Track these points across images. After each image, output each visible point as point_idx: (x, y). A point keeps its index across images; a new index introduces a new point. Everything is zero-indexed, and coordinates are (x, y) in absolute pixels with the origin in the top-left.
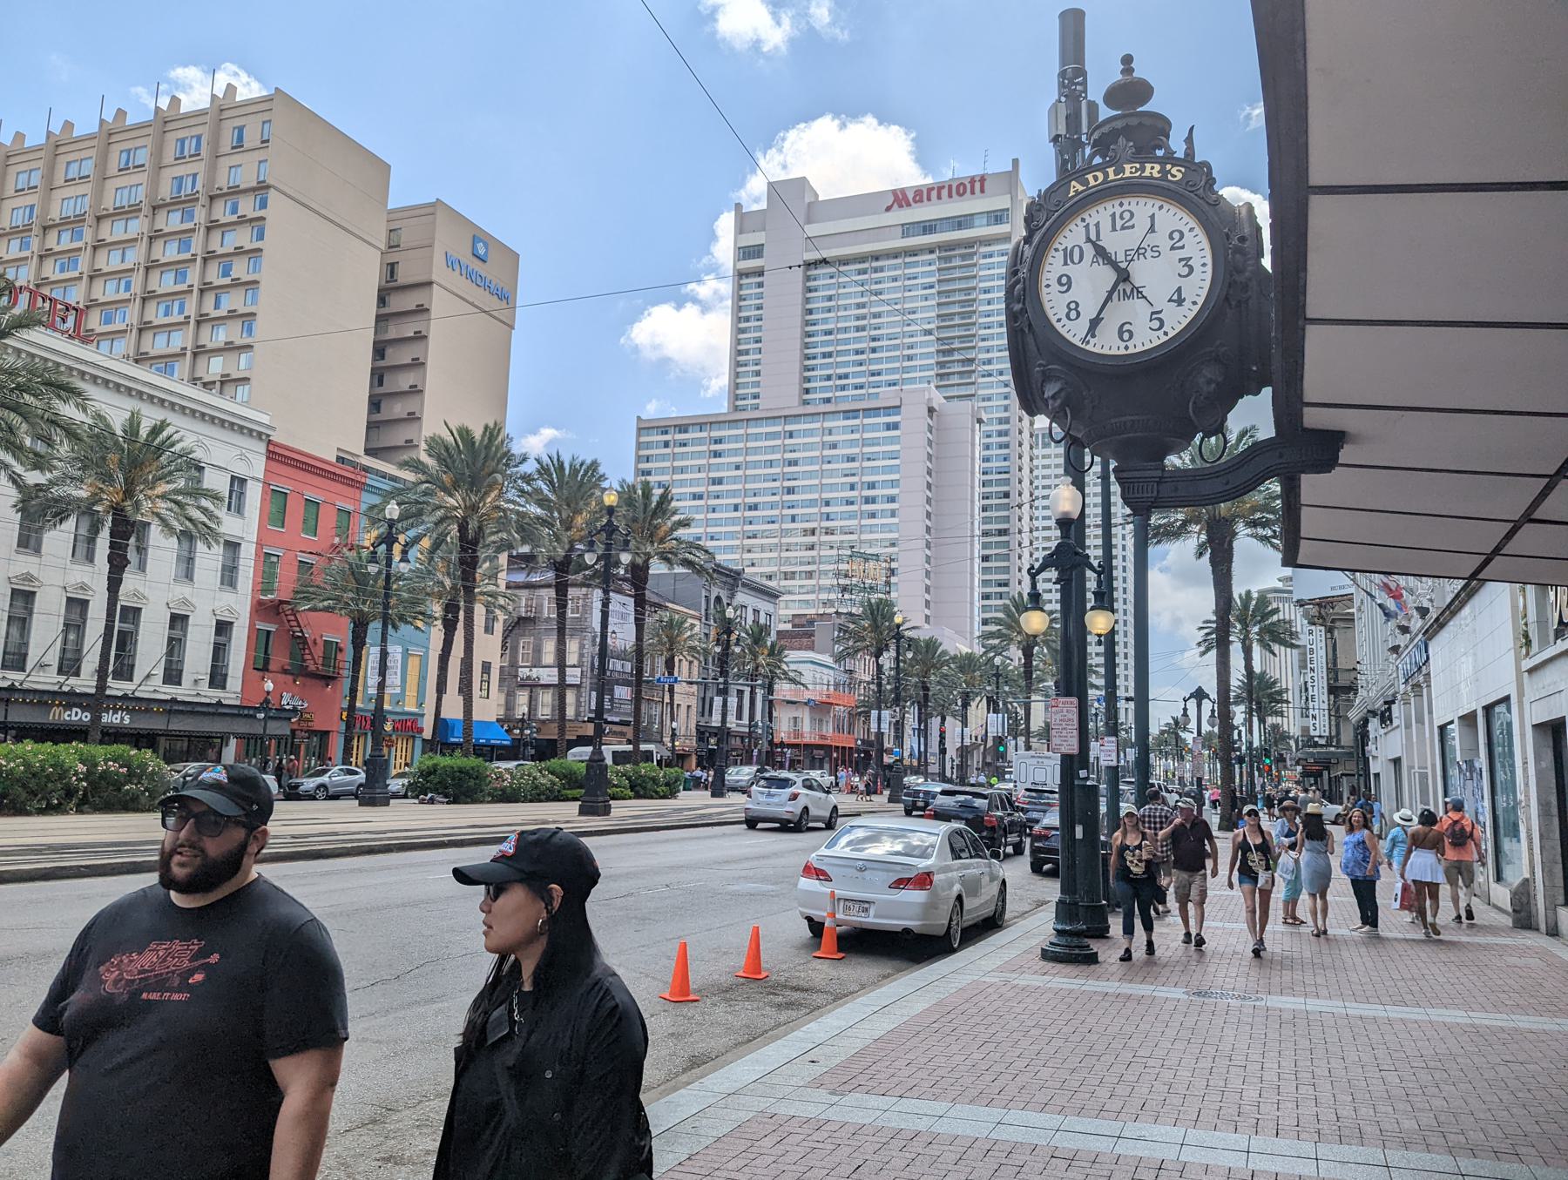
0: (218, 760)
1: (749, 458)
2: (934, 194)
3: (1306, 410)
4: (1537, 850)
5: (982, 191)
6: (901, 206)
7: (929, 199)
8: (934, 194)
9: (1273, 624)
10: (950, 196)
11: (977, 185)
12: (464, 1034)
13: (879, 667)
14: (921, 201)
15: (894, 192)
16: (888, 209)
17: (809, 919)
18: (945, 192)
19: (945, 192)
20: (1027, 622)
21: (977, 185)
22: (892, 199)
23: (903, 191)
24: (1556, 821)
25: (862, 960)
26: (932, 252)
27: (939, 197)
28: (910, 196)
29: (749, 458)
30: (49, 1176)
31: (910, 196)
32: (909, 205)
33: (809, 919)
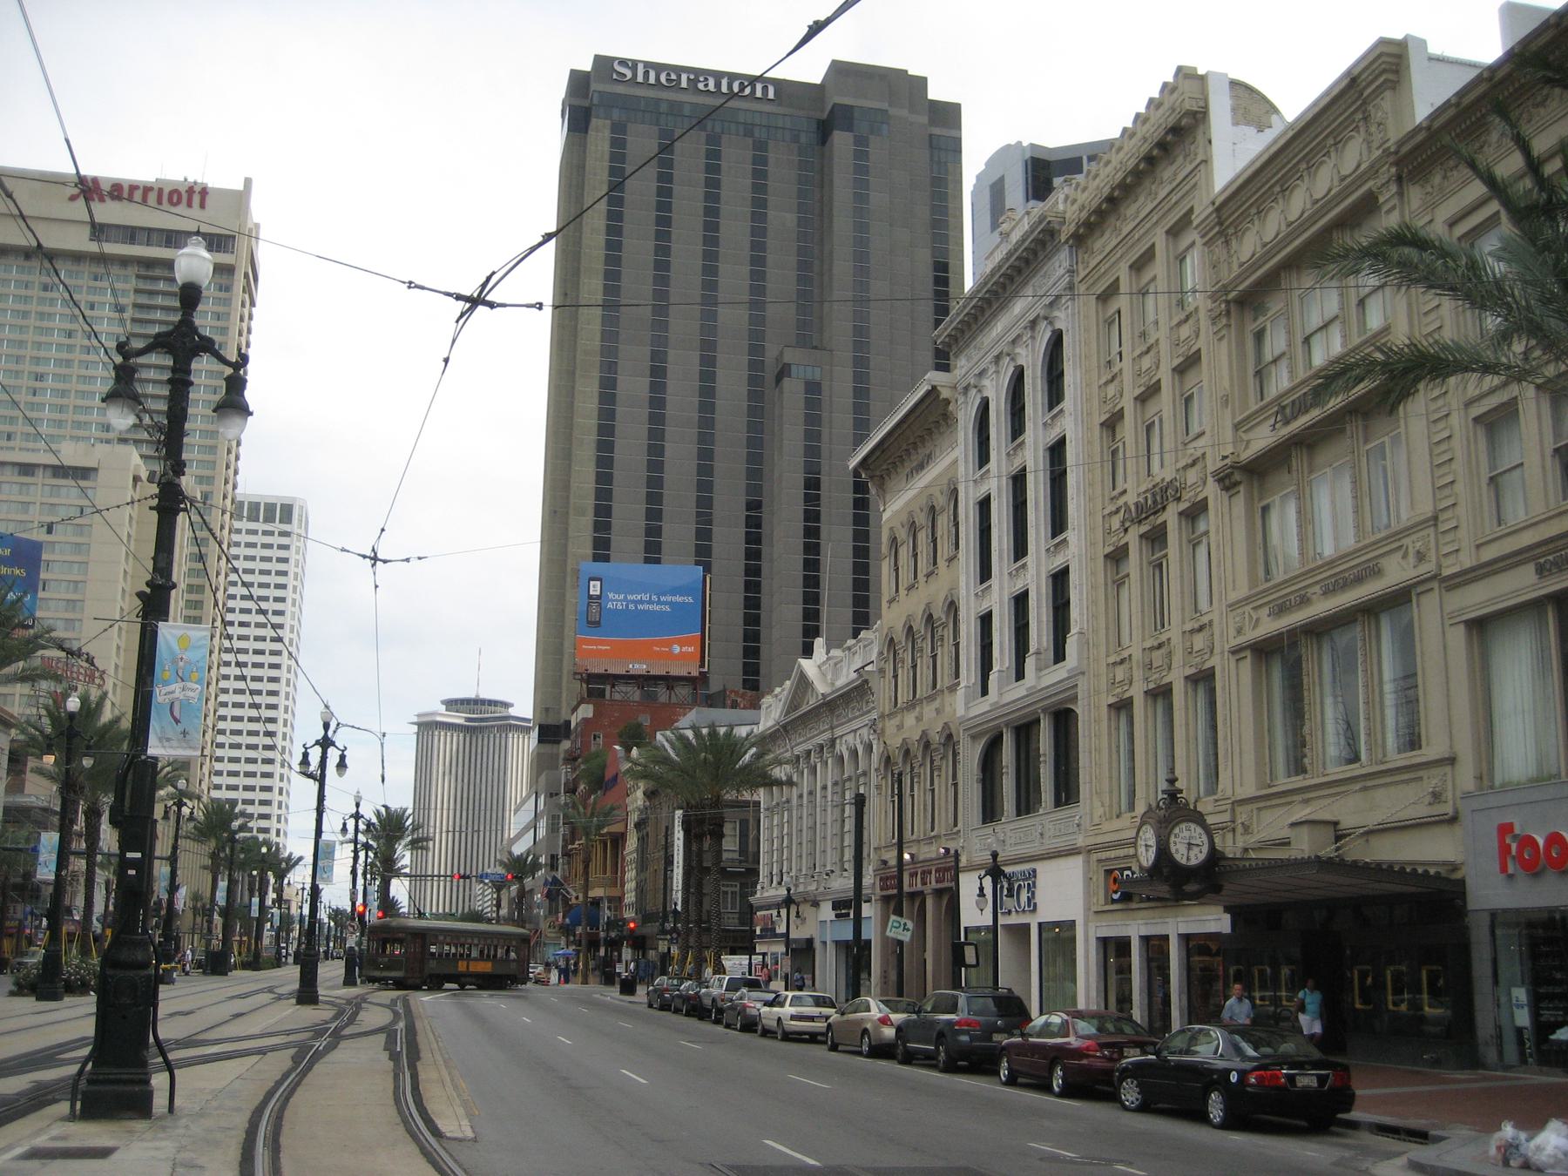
5: (202, 206)
11: (196, 199)
18: (152, 198)
21: (196, 199)
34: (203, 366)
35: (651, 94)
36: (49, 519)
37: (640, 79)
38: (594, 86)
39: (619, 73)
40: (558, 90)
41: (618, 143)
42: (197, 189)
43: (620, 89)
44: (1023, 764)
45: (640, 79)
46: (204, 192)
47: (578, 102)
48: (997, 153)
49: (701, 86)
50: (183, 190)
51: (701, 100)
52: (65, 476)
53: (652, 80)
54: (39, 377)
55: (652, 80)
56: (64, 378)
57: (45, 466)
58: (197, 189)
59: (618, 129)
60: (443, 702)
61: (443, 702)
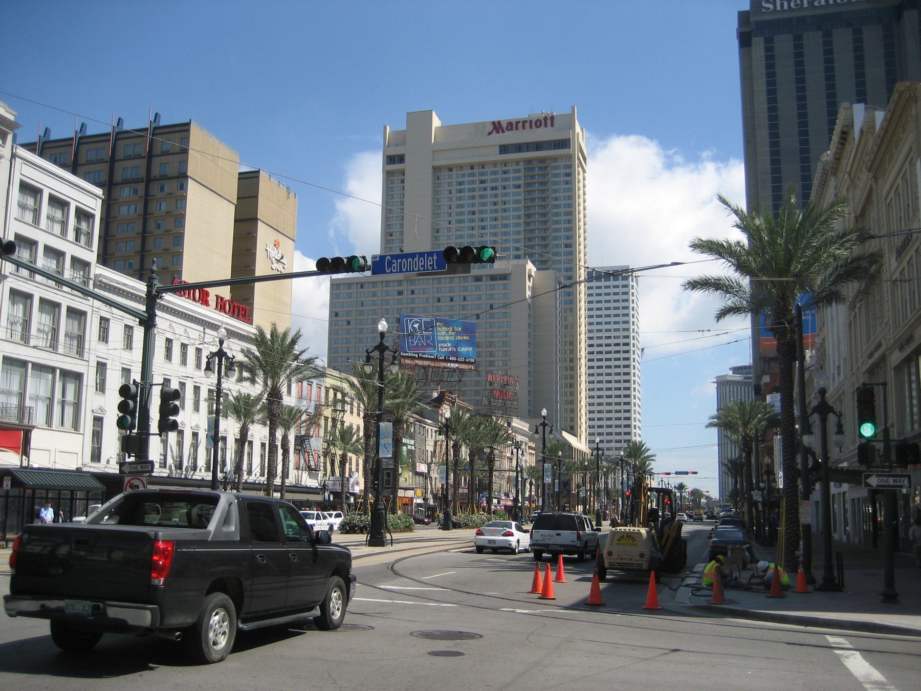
0: (329, 367)
2: (520, 125)
5: (552, 125)
7: (517, 129)
8: (520, 125)
10: (531, 127)
11: (549, 122)
12: (871, 664)
13: (674, 154)
14: (512, 129)
15: (493, 123)
17: (707, 427)
18: (527, 125)
19: (527, 125)
21: (549, 122)
22: (492, 127)
23: (499, 122)
24: (85, 383)
30: (918, 618)
31: (504, 125)
33: (707, 427)
34: (832, 418)
35: (785, 16)
36: (478, 312)
37: (778, 8)
38: (753, 19)
39: (765, 8)
40: (733, 24)
41: (769, 50)
42: (549, 117)
43: (767, 18)
44: (61, 144)
45: (778, 8)
46: (552, 118)
47: (745, 29)
48: (118, 676)
49: (816, 4)
50: (542, 119)
51: (817, 12)
52: (496, 279)
53: (786, 7)
54: (483, 228)
55: (786, 7)
56: (495, 227)
57: (393, 281)
58: (549, 117)
59: (769, 41)
60: (730, 369)
61: (730, 369)
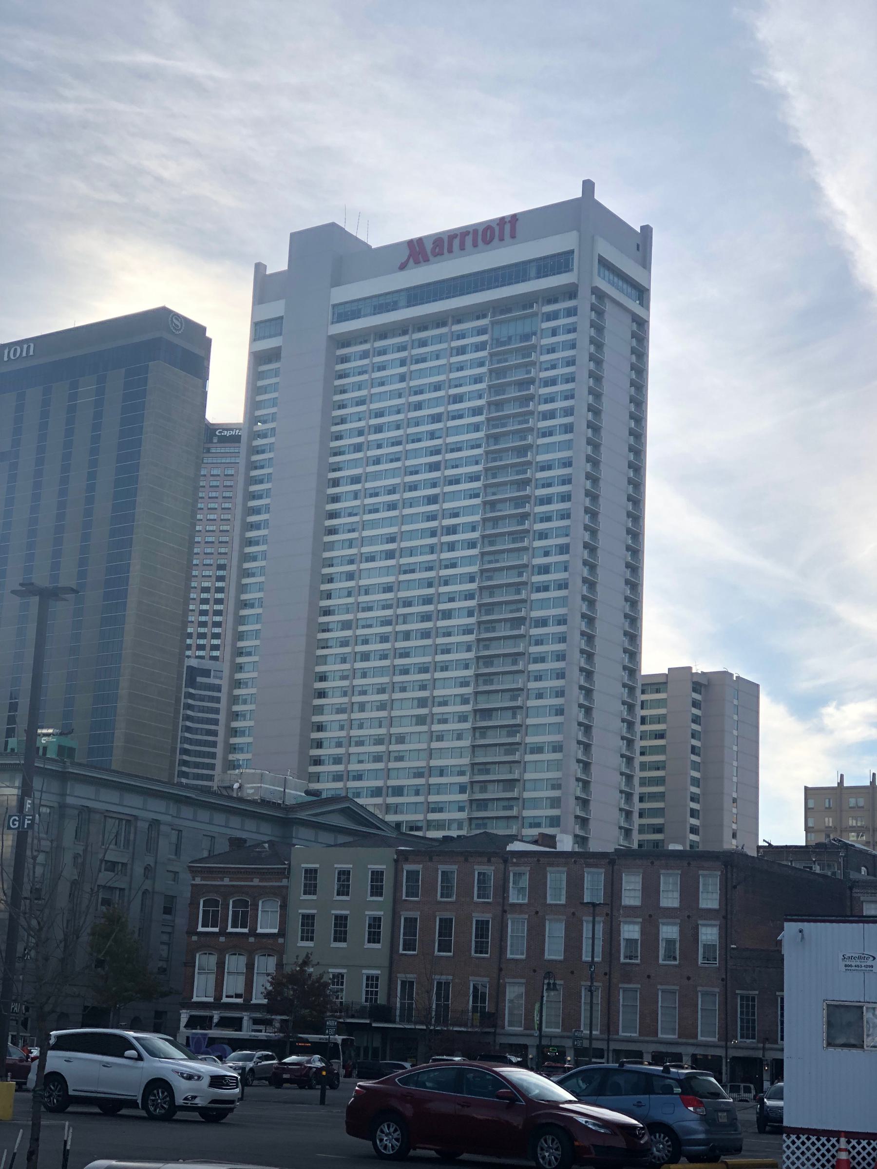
1: (405, 528)
2: (456, 243)
3: (846, 784)
4: (103, 1095)
5: (513, 236)
6: (417, 262)
7: (450, 251)
8: (456, 243)
9: (693, 1068)
10: (475, 245)
11: (507, 227)
15: (410, 243)
16: (403, 267)
18: (469, 240)
19: (469, 240)
20: (633, 878)
22: (407, 252)
25: (549, 1090)
26: (405, 332)
27: (462, 247)
28: (429, 247)
29: (405, 528)
31: (429, 247)
32: (427, 260)
